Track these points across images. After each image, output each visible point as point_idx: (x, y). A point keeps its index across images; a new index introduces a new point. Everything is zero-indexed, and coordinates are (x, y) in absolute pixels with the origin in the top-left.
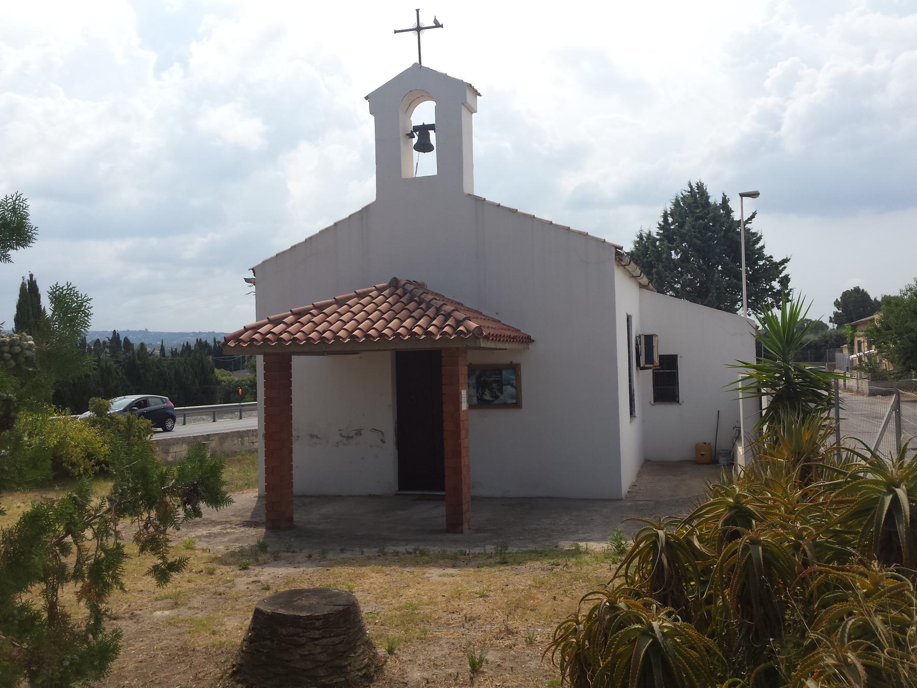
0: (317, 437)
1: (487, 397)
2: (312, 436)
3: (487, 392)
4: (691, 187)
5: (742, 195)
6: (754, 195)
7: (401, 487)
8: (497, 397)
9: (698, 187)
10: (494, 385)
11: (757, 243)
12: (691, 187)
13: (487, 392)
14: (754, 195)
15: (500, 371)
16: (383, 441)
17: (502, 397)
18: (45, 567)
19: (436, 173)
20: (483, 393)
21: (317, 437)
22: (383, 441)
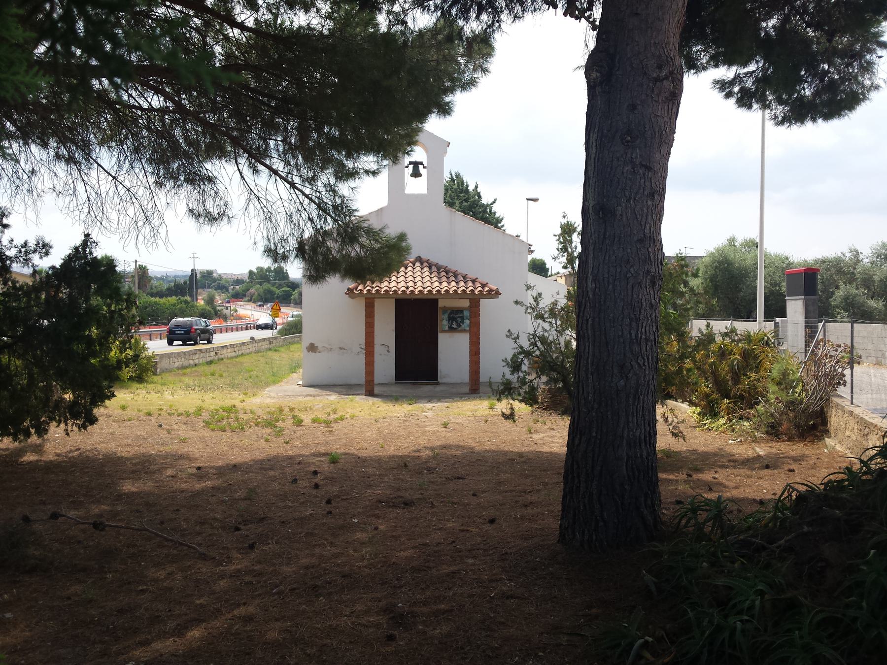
0: (344, 349)
1: (454, 326)
2: (341, 348)
3: (454, 323)
4: (451, 175)
5: (528, 199)
6: (535, 200)
7: (396, 380)
8: (460, 326)
9: (457, 176)
10: (459, 319)
11: (500, 223)
12: (451, 175)
13: (454, 323)
14: (535, 200)
15: (463, 311)
16: (388, 351)
17: (463, 326)
18: (444, 378)
19: (407, 192)
20: (452, 324)
21: (344, 349)
22: (388, 351)
